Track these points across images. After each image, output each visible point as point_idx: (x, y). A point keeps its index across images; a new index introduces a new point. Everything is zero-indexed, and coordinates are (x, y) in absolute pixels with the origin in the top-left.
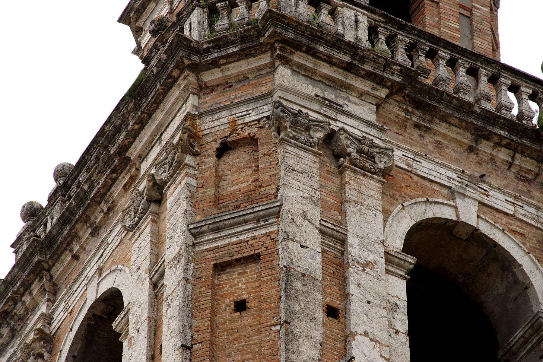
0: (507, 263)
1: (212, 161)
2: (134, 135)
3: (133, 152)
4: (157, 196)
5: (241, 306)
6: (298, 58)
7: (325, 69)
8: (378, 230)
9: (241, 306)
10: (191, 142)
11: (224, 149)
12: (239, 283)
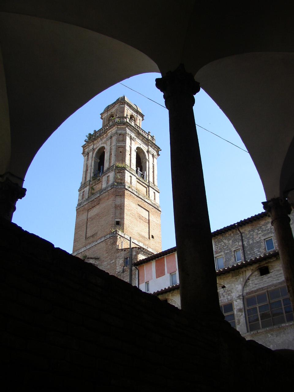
0: (144, 153)
1: (118, 136)
2: (108, 130)
3: (108, 132)
4: (111, 137)
5: (121, 152)
6: (129, 127)
7: (131, 129)
8: (134, 148)
9: (121, 152)
10: (116, 133)
11: (120, 135)
12: (121, 149)
